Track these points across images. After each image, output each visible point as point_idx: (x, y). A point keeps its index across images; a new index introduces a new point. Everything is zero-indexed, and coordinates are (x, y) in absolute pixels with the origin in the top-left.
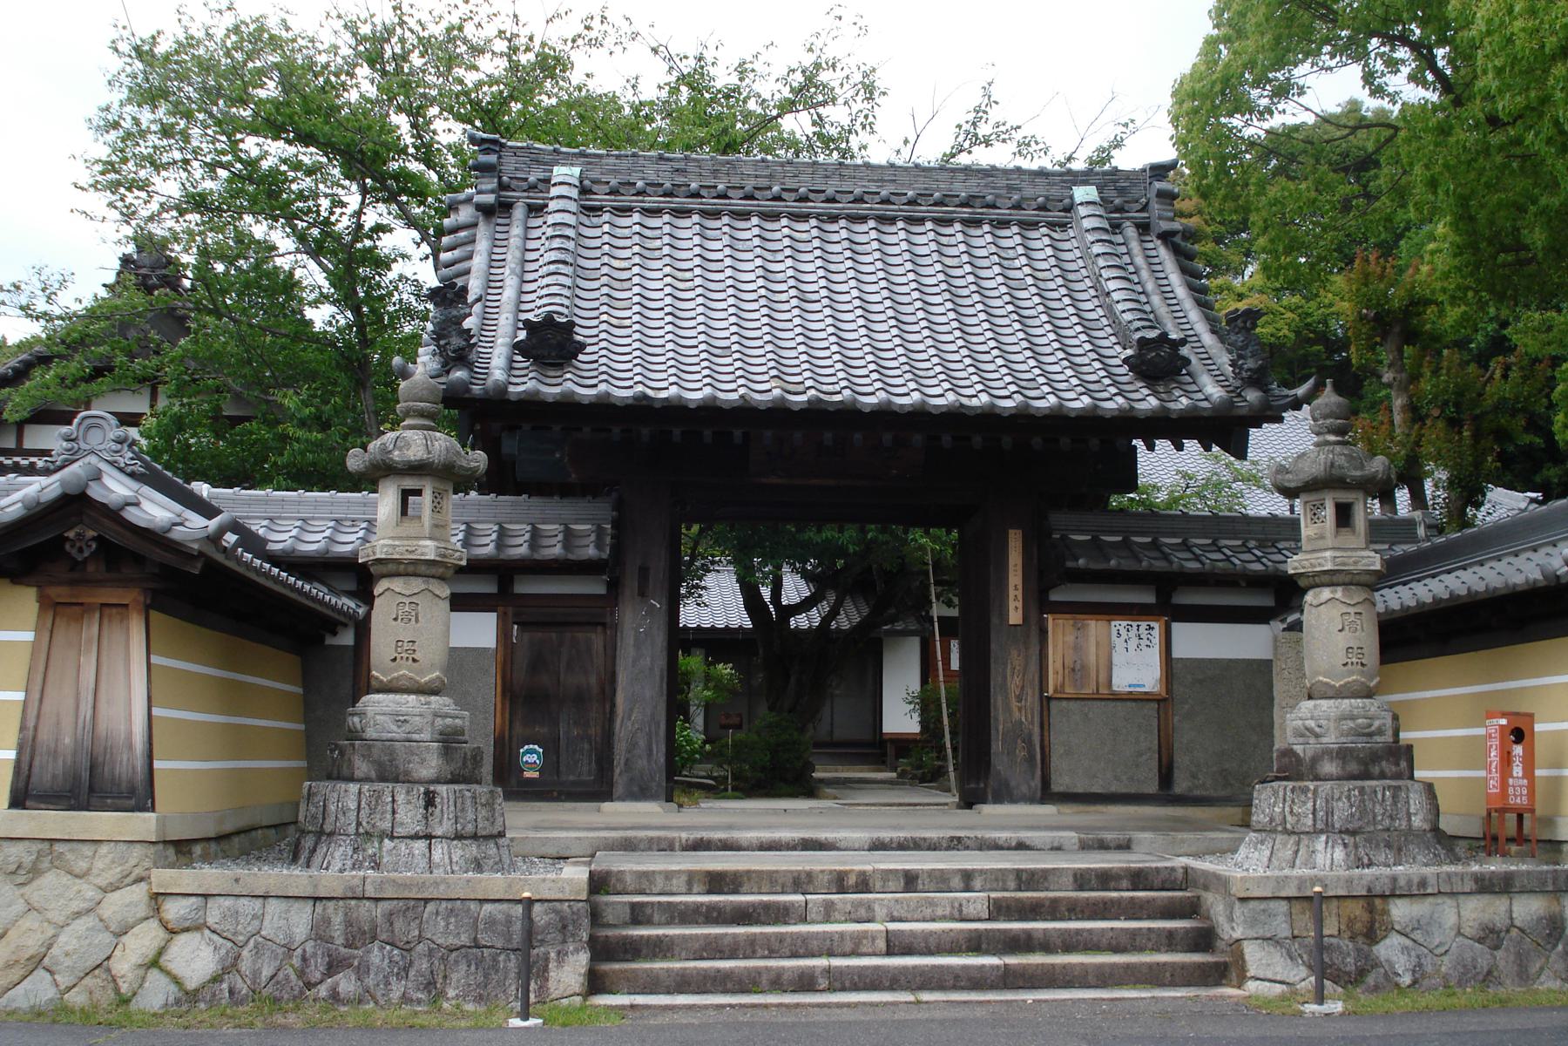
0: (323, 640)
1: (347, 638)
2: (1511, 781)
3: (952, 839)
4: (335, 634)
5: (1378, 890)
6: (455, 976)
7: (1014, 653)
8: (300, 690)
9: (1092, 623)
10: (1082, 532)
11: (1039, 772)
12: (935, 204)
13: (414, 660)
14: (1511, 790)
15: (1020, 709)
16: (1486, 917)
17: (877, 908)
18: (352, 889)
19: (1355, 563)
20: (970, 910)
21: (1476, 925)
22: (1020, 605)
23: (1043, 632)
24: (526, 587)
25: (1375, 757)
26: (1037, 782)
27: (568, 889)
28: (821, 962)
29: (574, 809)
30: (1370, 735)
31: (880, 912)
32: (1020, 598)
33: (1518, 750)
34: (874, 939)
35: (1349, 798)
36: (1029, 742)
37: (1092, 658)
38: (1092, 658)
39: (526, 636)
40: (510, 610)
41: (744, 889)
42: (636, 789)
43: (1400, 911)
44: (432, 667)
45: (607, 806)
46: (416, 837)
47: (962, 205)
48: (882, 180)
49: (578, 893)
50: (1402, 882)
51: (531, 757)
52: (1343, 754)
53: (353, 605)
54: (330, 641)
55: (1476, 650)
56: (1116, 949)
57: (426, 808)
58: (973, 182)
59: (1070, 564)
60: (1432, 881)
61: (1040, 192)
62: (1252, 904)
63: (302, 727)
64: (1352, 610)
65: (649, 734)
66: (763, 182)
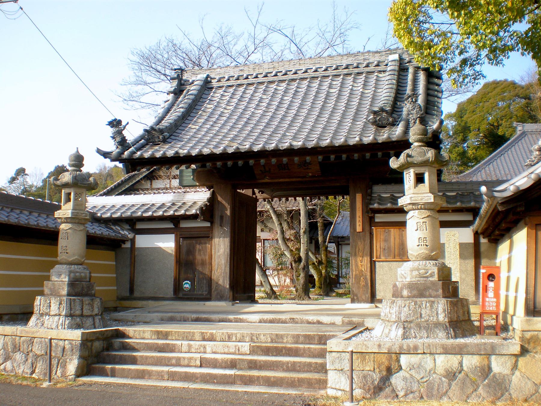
0: (121, 245)
1: (128, 245)
2: (487, 299)
3: (291, 319)
4: (124, 244)
5: (393, 350)
6: (38, 365)
7: (359, 243)
8: (114, 263)
9: (392, 230)
10: (386, 193)
11: (369, 291)
12: (334, 70)
13: (67, 253)
14: (487, 304)
15: (362, 265)
16: (448, 366)
17: (207, 347)
18: (14, 332)
19: (421, 199)
20: (243, 350)
21: (443, 368)
22: (361, 224)
23: (371, 234)
24: (184, 225)
25: (426, 288)
26: (369, 295)
27: (75, 336)
28: (166, 369)
29: (199, 304)
30: (427, 277)
31: (208, 350)
32: (361, 221)
33: (491, 284)
34: (196, 360)
35: (409, 307)
36: (365, 279)
37: (392, 244)
38: (392, 244)
39: (185, 242)
40: (178, 233)
41: (169, 338)
42: (219, 297)
43: (404, 360)
44: (74, 255)
45: (208, 303)
46: (56, 315)
47: (345, 68)
48: (315, 63)
49: (78, 338)
50: (405, 347)
51: (187, 285)
52: (411, 286)
53: (127, 233)
54: (123, 246)
55: (14, 241)
56: (288, 370)
57: (59, 305)
58: (350, 59)
59: (371, 206)
60: (421, 347)
61: (374, 60)
62: (334, 354)
63: (115, 275)
64: (422, 221)
65: (224, 277)
66: (270, 71)
